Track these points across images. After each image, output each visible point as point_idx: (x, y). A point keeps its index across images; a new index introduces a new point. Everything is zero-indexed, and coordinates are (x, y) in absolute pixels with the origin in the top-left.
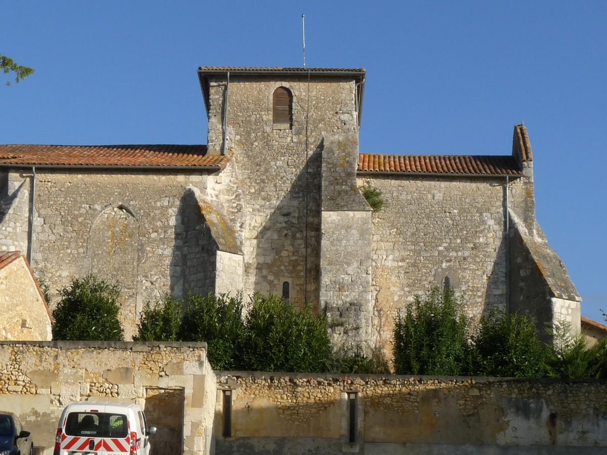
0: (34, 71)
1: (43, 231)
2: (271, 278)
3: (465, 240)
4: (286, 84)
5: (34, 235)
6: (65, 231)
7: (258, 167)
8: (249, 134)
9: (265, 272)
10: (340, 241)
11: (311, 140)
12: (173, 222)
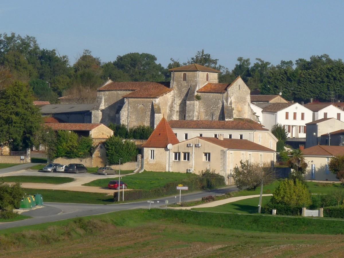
0: (240, 59)
1: (130, 109)
2: (182, 113)
3: (216, 106)
4: (185, 72)
5: (129, 110)
6: (134, 109)
7: (180, 90)
8: (178, 83)
9: (181, 112)
10: (189, 107)
11: (189, 84)
12: (150, 108)
